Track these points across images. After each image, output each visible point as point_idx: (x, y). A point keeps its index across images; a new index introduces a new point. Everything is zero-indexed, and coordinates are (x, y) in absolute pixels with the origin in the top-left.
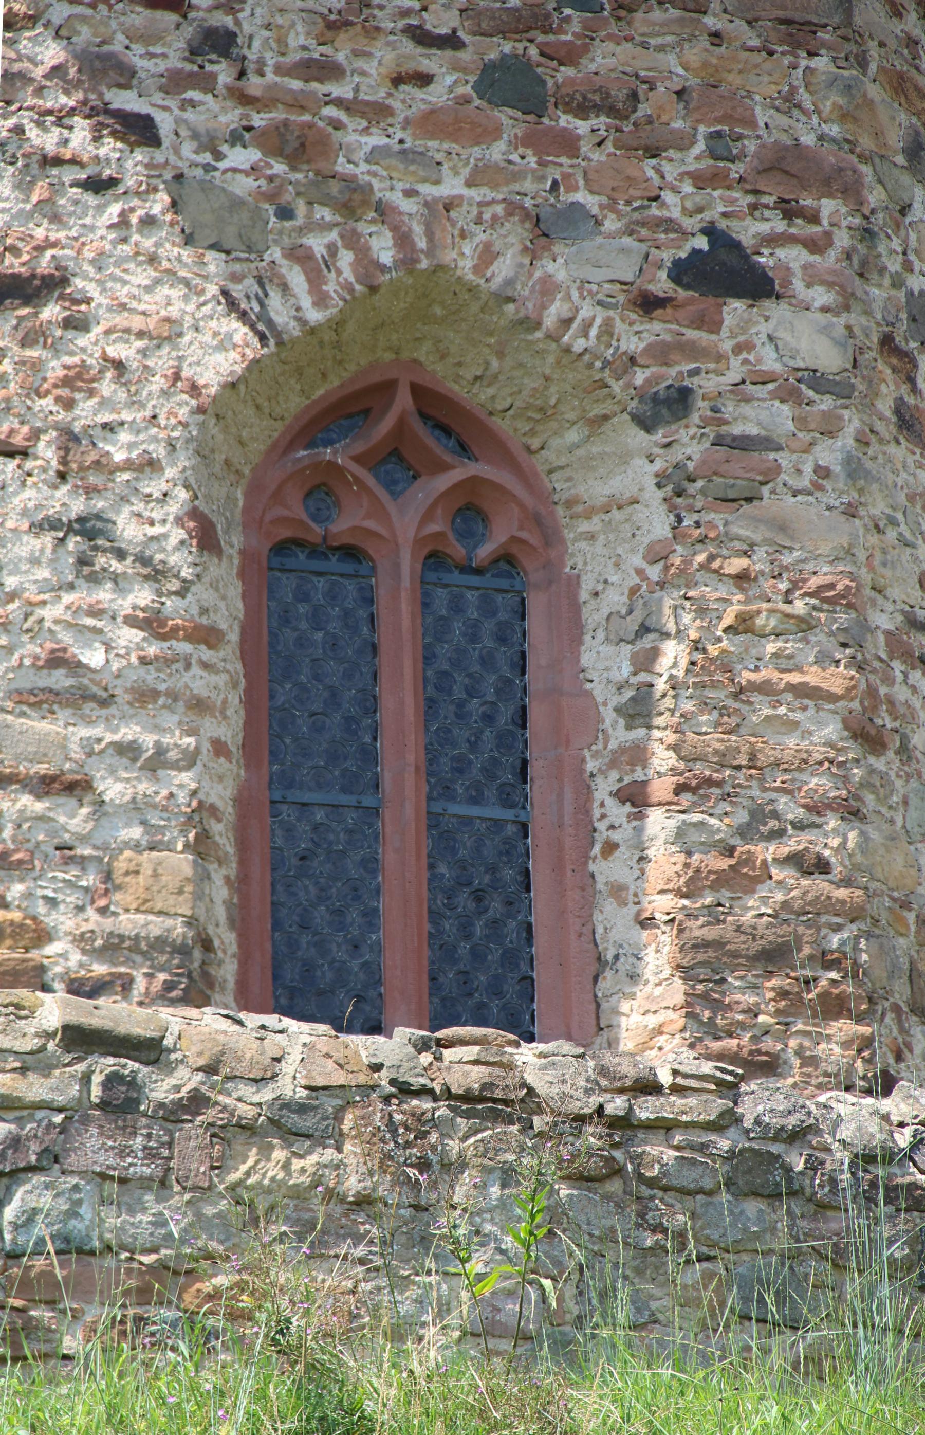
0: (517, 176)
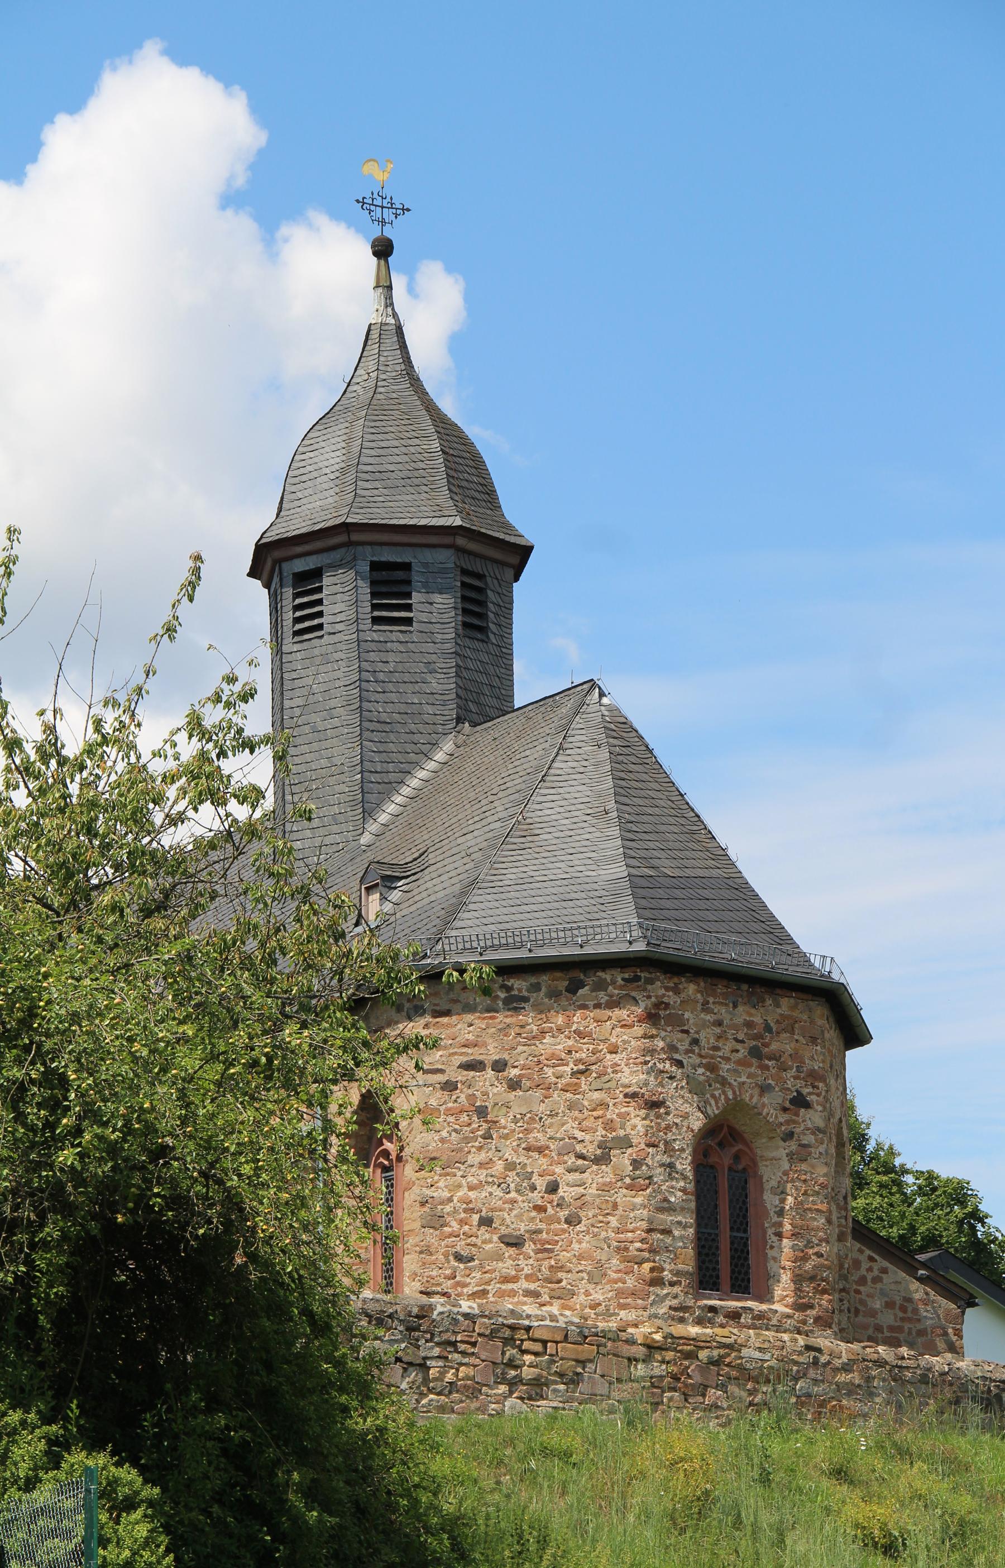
0: (757, 1076)
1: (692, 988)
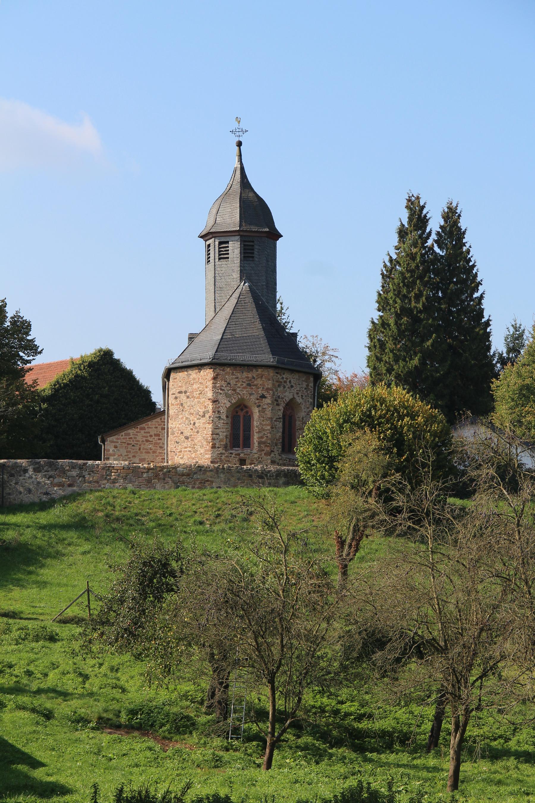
1: (229, 369)
